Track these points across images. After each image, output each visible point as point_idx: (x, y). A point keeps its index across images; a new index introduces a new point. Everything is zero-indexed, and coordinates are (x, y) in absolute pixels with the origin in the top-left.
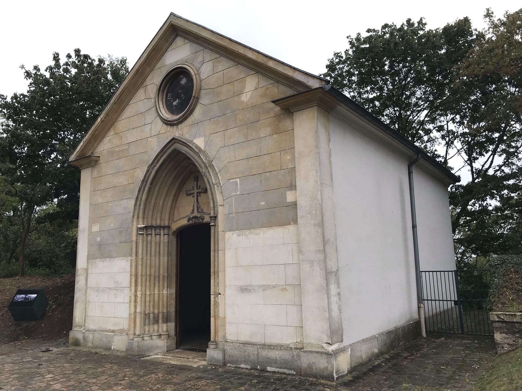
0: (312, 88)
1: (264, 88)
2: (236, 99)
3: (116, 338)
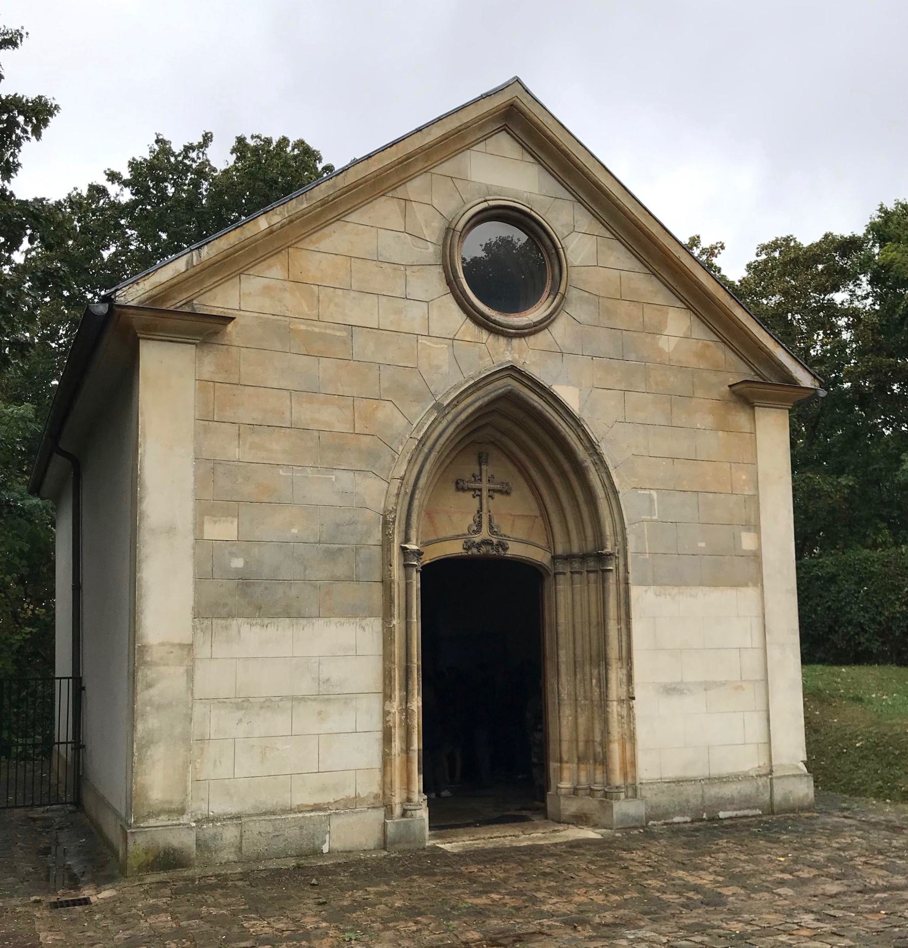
1: (700, 342)
2: (649, 339)
3: (335, 822)
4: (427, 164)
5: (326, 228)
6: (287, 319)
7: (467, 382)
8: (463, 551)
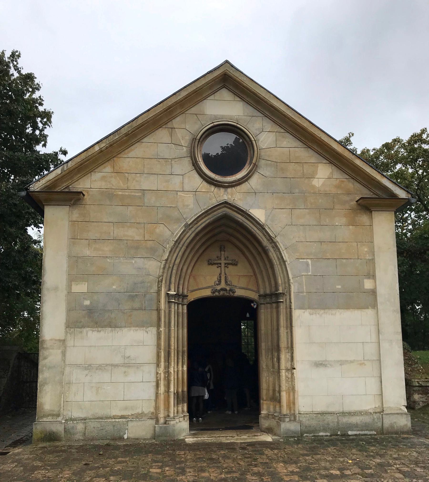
0: (398, 197)
1: (338, 180)
2: (306, 181)
3: (130, 424)
4: (182, 110)
6: (113, 190)
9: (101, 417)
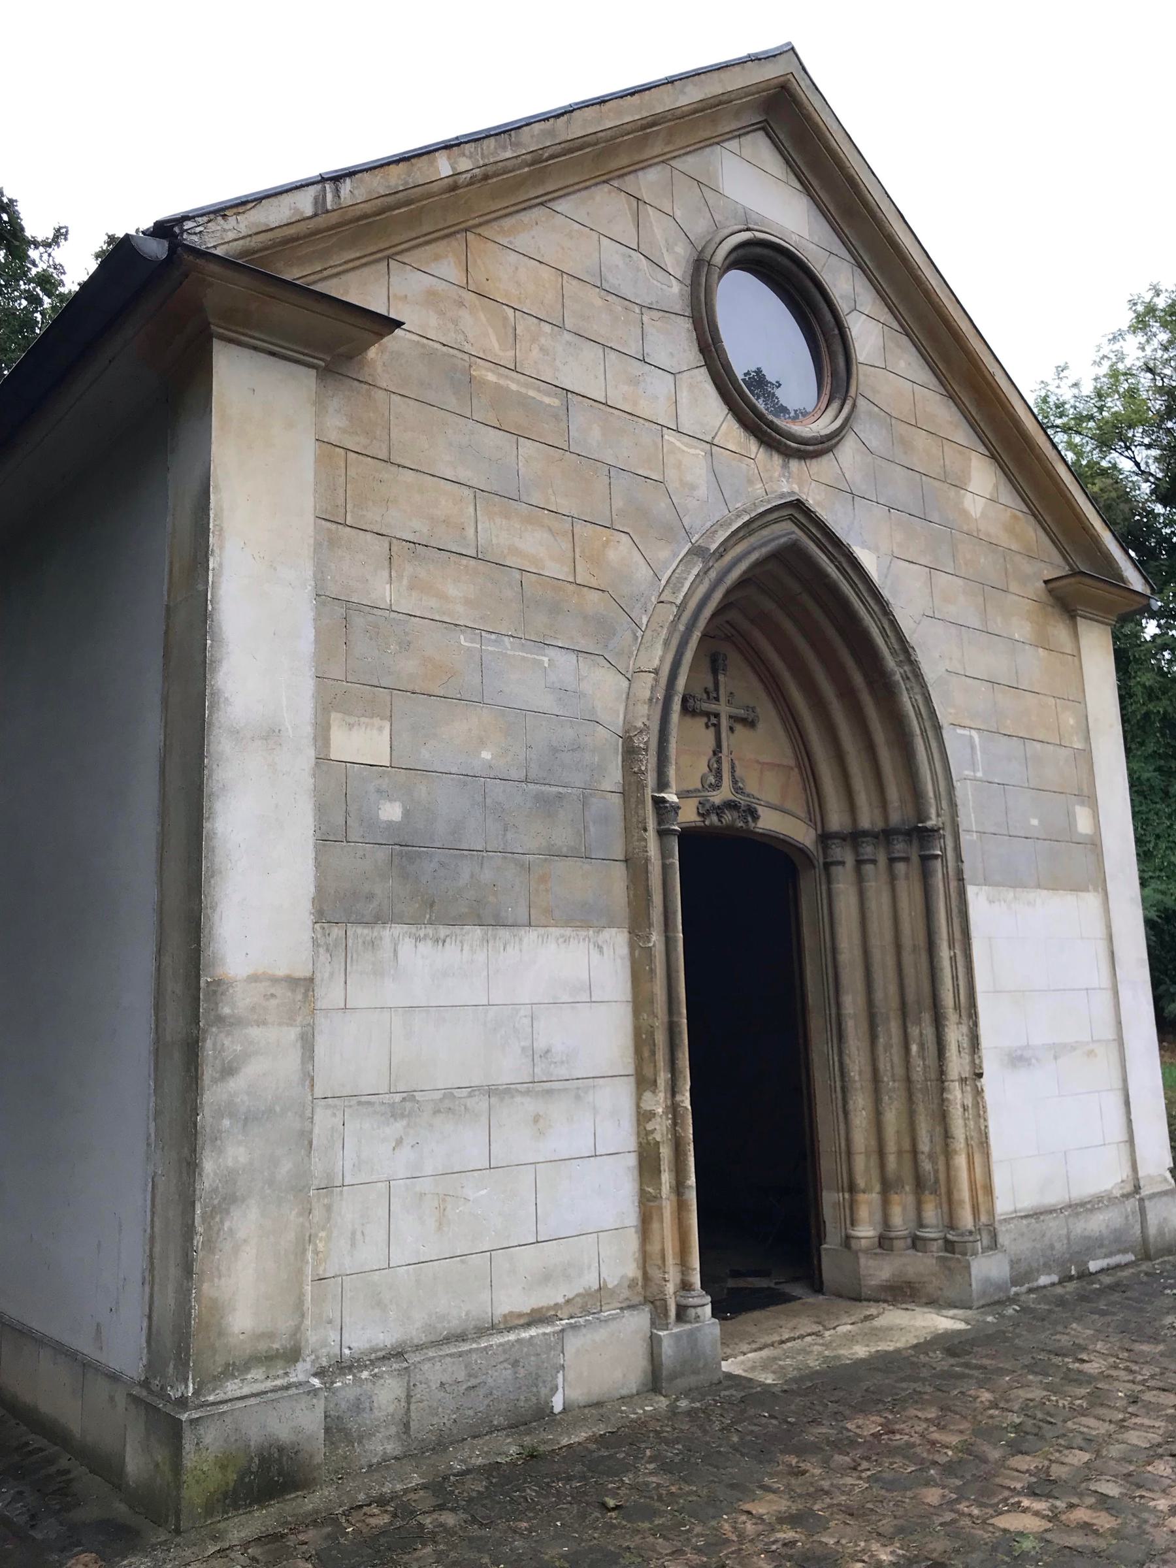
2: (952, 492)
3: (573, 1343)
4: (666, 150)
5: (523, 214)
7: (738, 516)
8: (698, 819)
9: (459, 1331)
